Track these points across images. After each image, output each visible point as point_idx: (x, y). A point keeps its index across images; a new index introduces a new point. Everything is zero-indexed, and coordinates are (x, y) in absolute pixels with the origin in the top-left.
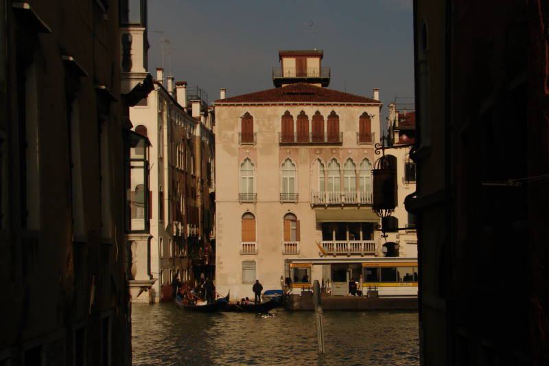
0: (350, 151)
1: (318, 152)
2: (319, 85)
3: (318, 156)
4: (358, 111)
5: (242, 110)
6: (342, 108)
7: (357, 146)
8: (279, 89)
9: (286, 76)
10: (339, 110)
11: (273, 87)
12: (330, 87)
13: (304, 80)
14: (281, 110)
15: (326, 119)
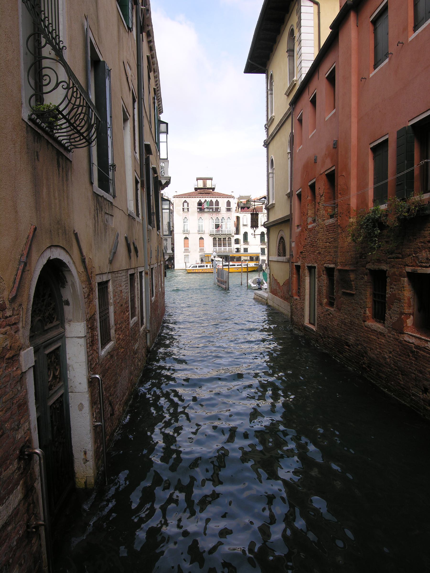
0: (223, 215)
1: (211, 215)
2: (211, 190)
3: (211, 217)
4: (226, 200)
5: (184, 199)
6: (220, 198)
7: (225, 213)
8: (196, 192)
9: (199, 187)
10: (219, 199)
11: (194, 191)
12: (215, 191)
13: (205, 188)
14: (197, 200)
15: (214, 203)
